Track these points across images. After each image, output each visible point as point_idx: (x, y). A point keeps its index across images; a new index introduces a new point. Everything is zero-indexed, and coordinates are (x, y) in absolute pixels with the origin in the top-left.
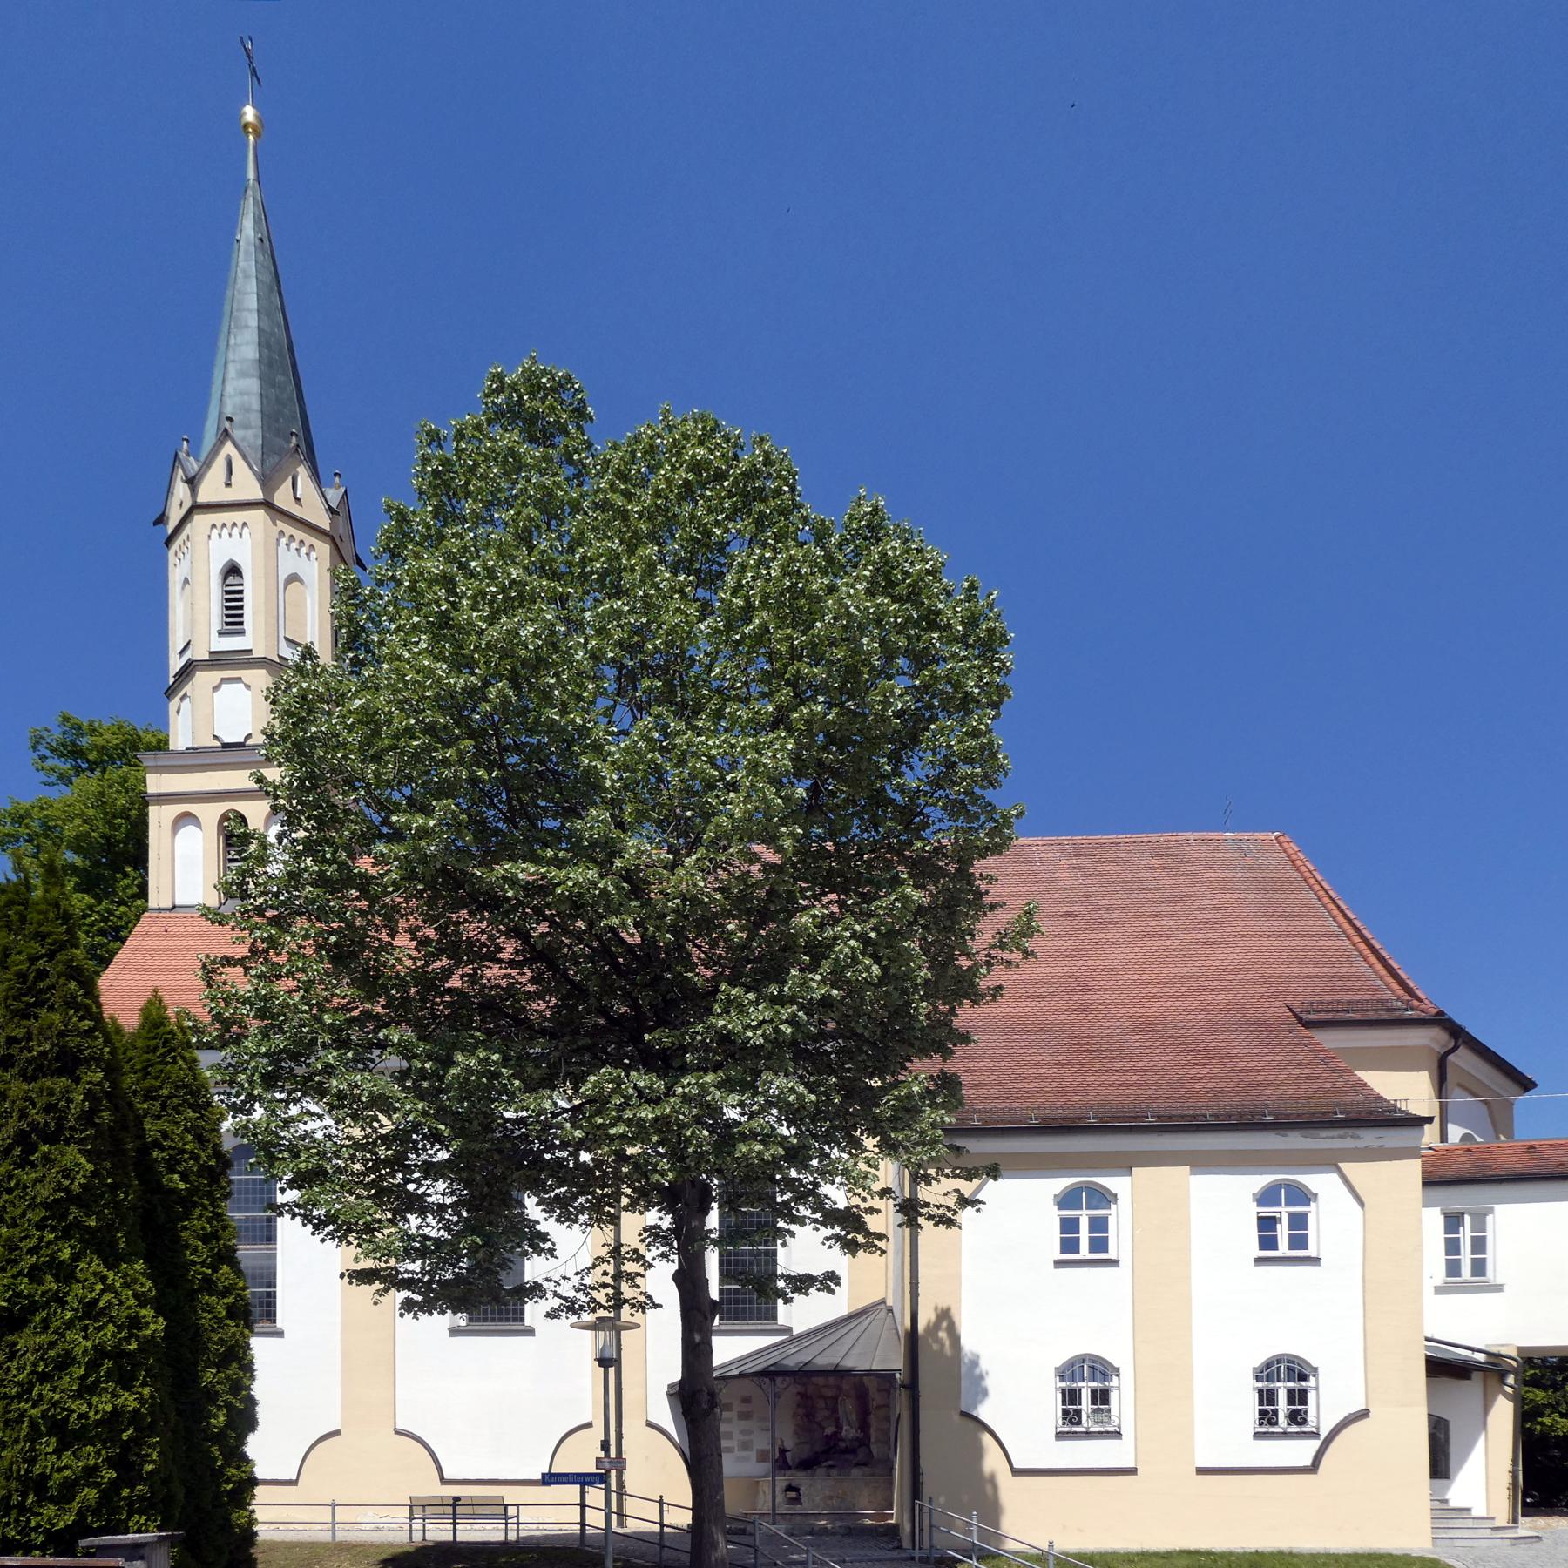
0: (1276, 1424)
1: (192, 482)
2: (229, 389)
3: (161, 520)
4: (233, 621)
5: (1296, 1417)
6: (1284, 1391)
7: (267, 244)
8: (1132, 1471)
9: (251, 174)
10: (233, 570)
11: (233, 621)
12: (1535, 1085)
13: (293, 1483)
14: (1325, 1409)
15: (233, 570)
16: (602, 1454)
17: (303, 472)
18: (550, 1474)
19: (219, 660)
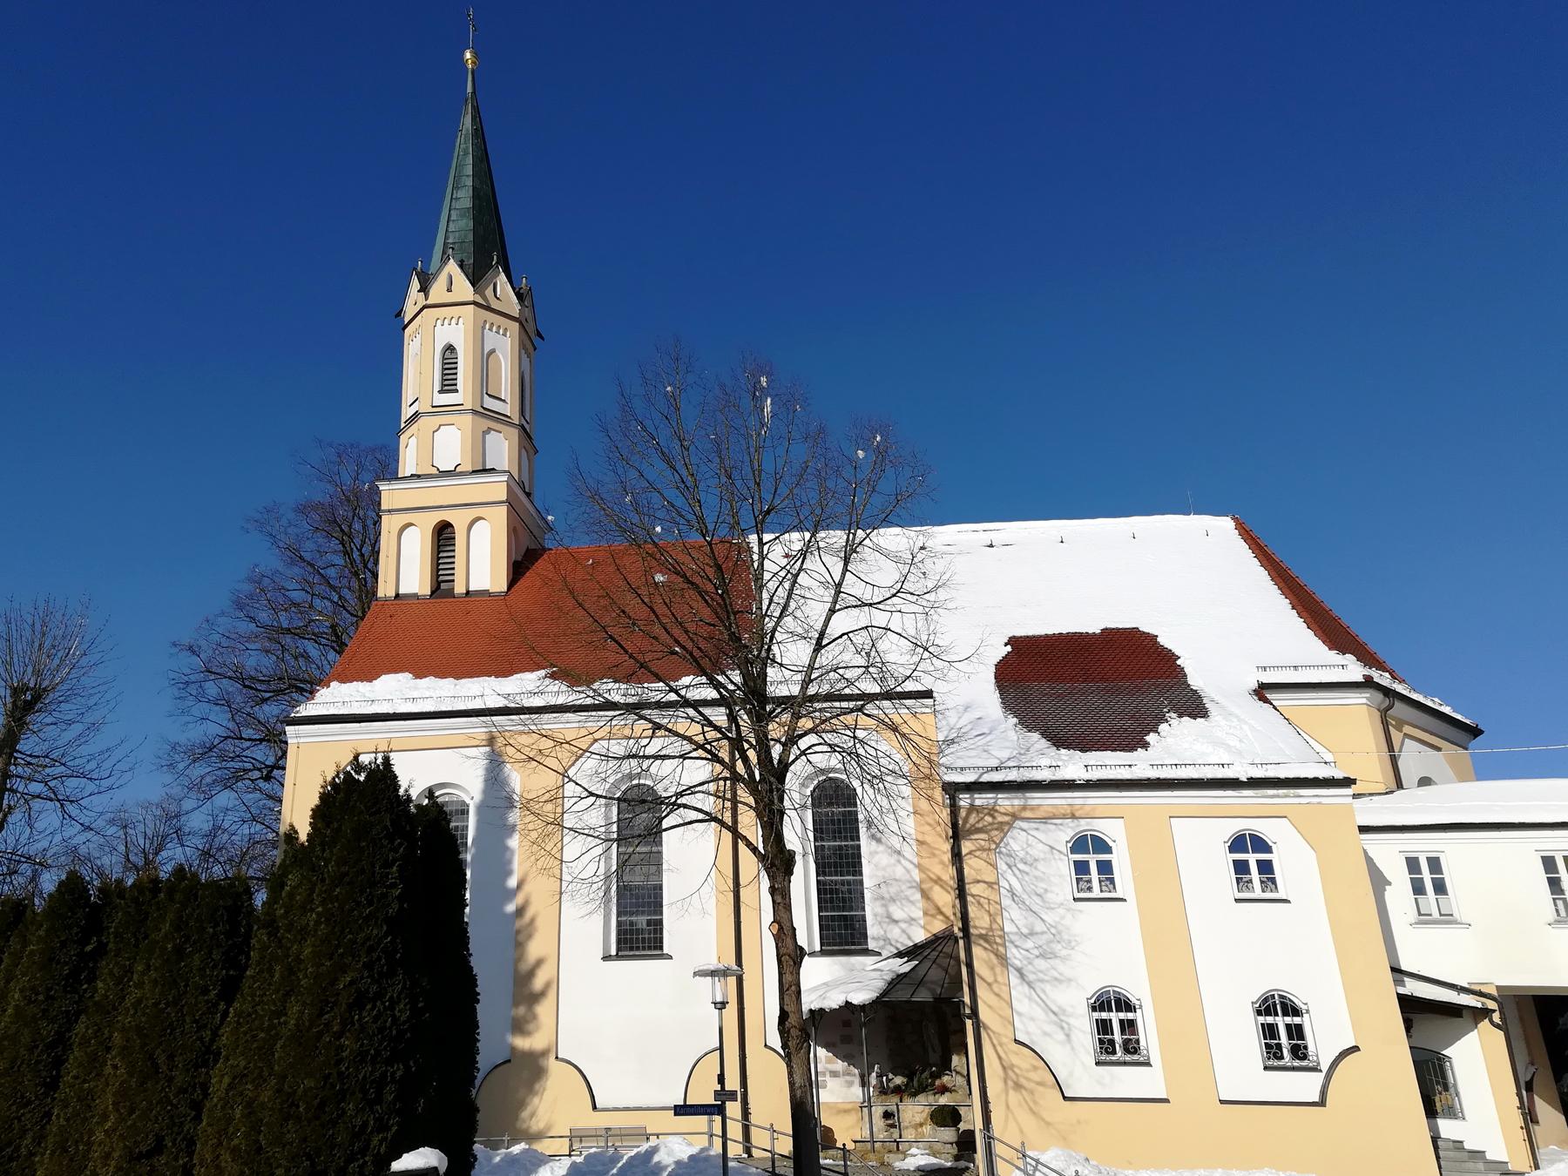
0: (1282, 1058)
1: (424, 289)
2: (452, 227)
3: (399, 314)
4: (448, 385)
5: (1299, 1052)
6: (1282, 1030)
7: (479, 133)
8: (1166, 1101)
9: (469, 90)
10: (450, 348)
11: (448, 385)
12: (1481, 732)
13: (595, 1107)
14: (1323, 1042)
15: (450, 348)
16: (718, 1087)
17: (503, 276)
18: (685, 1106)
19: (438, 410)
